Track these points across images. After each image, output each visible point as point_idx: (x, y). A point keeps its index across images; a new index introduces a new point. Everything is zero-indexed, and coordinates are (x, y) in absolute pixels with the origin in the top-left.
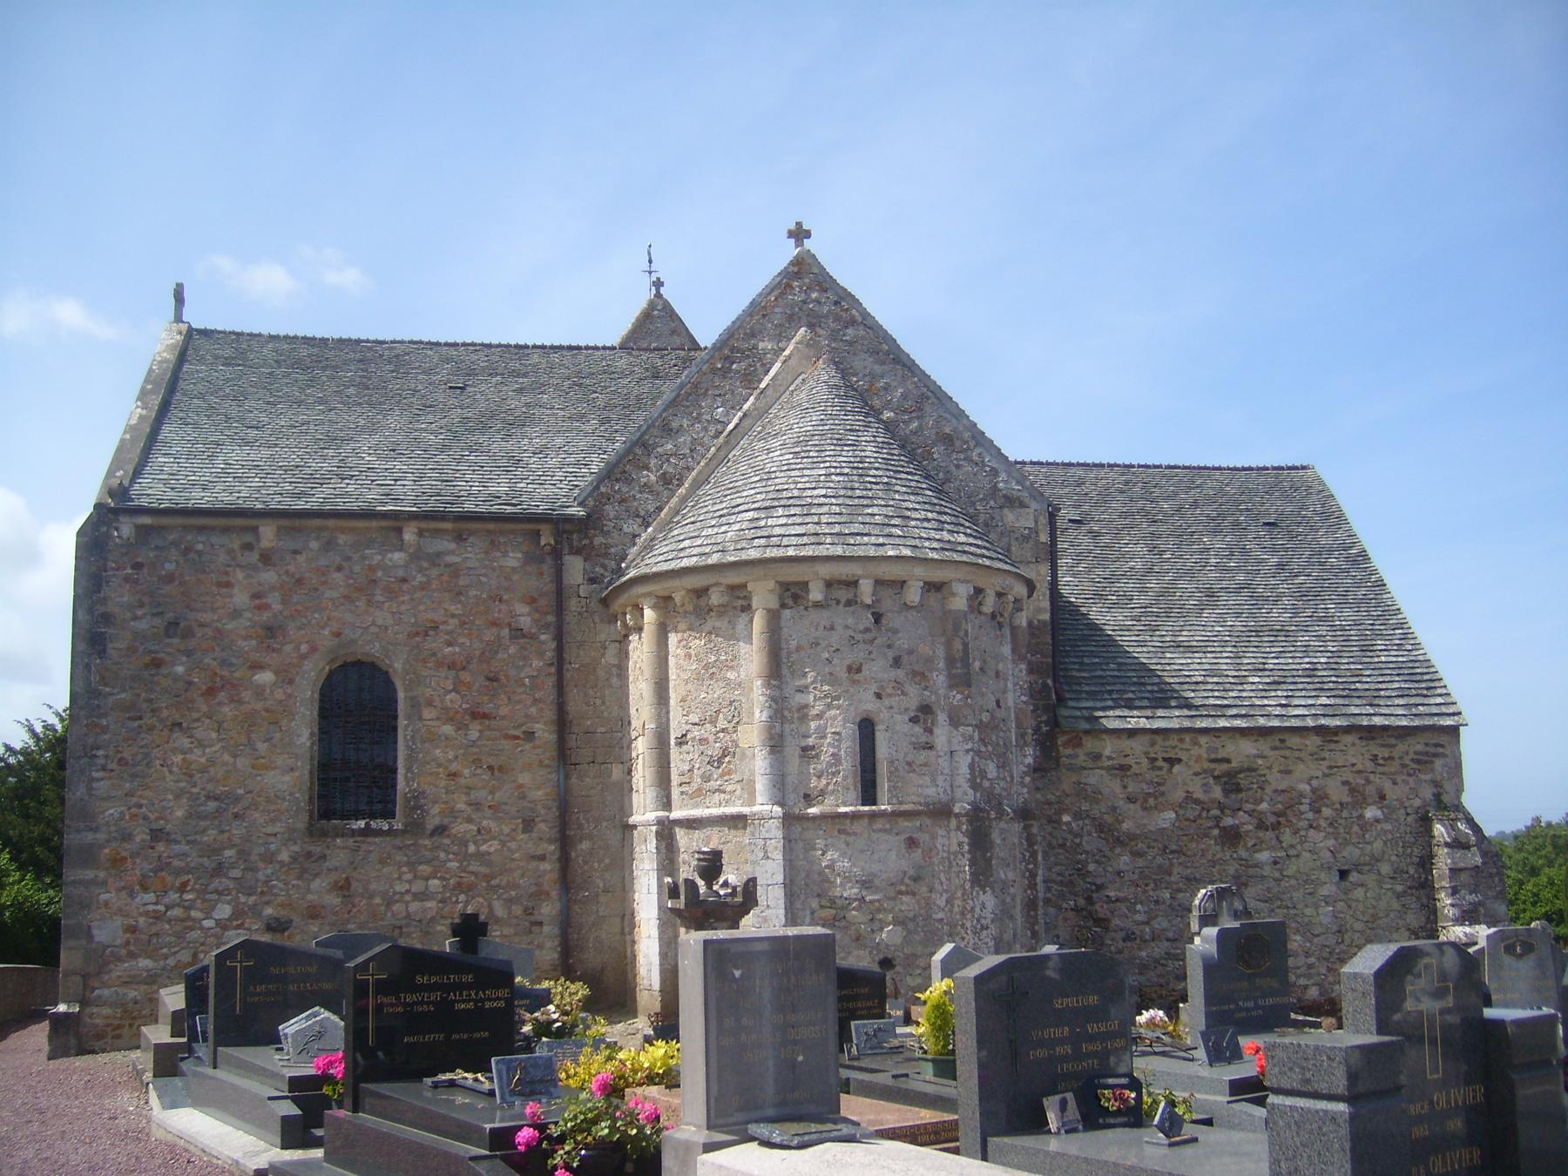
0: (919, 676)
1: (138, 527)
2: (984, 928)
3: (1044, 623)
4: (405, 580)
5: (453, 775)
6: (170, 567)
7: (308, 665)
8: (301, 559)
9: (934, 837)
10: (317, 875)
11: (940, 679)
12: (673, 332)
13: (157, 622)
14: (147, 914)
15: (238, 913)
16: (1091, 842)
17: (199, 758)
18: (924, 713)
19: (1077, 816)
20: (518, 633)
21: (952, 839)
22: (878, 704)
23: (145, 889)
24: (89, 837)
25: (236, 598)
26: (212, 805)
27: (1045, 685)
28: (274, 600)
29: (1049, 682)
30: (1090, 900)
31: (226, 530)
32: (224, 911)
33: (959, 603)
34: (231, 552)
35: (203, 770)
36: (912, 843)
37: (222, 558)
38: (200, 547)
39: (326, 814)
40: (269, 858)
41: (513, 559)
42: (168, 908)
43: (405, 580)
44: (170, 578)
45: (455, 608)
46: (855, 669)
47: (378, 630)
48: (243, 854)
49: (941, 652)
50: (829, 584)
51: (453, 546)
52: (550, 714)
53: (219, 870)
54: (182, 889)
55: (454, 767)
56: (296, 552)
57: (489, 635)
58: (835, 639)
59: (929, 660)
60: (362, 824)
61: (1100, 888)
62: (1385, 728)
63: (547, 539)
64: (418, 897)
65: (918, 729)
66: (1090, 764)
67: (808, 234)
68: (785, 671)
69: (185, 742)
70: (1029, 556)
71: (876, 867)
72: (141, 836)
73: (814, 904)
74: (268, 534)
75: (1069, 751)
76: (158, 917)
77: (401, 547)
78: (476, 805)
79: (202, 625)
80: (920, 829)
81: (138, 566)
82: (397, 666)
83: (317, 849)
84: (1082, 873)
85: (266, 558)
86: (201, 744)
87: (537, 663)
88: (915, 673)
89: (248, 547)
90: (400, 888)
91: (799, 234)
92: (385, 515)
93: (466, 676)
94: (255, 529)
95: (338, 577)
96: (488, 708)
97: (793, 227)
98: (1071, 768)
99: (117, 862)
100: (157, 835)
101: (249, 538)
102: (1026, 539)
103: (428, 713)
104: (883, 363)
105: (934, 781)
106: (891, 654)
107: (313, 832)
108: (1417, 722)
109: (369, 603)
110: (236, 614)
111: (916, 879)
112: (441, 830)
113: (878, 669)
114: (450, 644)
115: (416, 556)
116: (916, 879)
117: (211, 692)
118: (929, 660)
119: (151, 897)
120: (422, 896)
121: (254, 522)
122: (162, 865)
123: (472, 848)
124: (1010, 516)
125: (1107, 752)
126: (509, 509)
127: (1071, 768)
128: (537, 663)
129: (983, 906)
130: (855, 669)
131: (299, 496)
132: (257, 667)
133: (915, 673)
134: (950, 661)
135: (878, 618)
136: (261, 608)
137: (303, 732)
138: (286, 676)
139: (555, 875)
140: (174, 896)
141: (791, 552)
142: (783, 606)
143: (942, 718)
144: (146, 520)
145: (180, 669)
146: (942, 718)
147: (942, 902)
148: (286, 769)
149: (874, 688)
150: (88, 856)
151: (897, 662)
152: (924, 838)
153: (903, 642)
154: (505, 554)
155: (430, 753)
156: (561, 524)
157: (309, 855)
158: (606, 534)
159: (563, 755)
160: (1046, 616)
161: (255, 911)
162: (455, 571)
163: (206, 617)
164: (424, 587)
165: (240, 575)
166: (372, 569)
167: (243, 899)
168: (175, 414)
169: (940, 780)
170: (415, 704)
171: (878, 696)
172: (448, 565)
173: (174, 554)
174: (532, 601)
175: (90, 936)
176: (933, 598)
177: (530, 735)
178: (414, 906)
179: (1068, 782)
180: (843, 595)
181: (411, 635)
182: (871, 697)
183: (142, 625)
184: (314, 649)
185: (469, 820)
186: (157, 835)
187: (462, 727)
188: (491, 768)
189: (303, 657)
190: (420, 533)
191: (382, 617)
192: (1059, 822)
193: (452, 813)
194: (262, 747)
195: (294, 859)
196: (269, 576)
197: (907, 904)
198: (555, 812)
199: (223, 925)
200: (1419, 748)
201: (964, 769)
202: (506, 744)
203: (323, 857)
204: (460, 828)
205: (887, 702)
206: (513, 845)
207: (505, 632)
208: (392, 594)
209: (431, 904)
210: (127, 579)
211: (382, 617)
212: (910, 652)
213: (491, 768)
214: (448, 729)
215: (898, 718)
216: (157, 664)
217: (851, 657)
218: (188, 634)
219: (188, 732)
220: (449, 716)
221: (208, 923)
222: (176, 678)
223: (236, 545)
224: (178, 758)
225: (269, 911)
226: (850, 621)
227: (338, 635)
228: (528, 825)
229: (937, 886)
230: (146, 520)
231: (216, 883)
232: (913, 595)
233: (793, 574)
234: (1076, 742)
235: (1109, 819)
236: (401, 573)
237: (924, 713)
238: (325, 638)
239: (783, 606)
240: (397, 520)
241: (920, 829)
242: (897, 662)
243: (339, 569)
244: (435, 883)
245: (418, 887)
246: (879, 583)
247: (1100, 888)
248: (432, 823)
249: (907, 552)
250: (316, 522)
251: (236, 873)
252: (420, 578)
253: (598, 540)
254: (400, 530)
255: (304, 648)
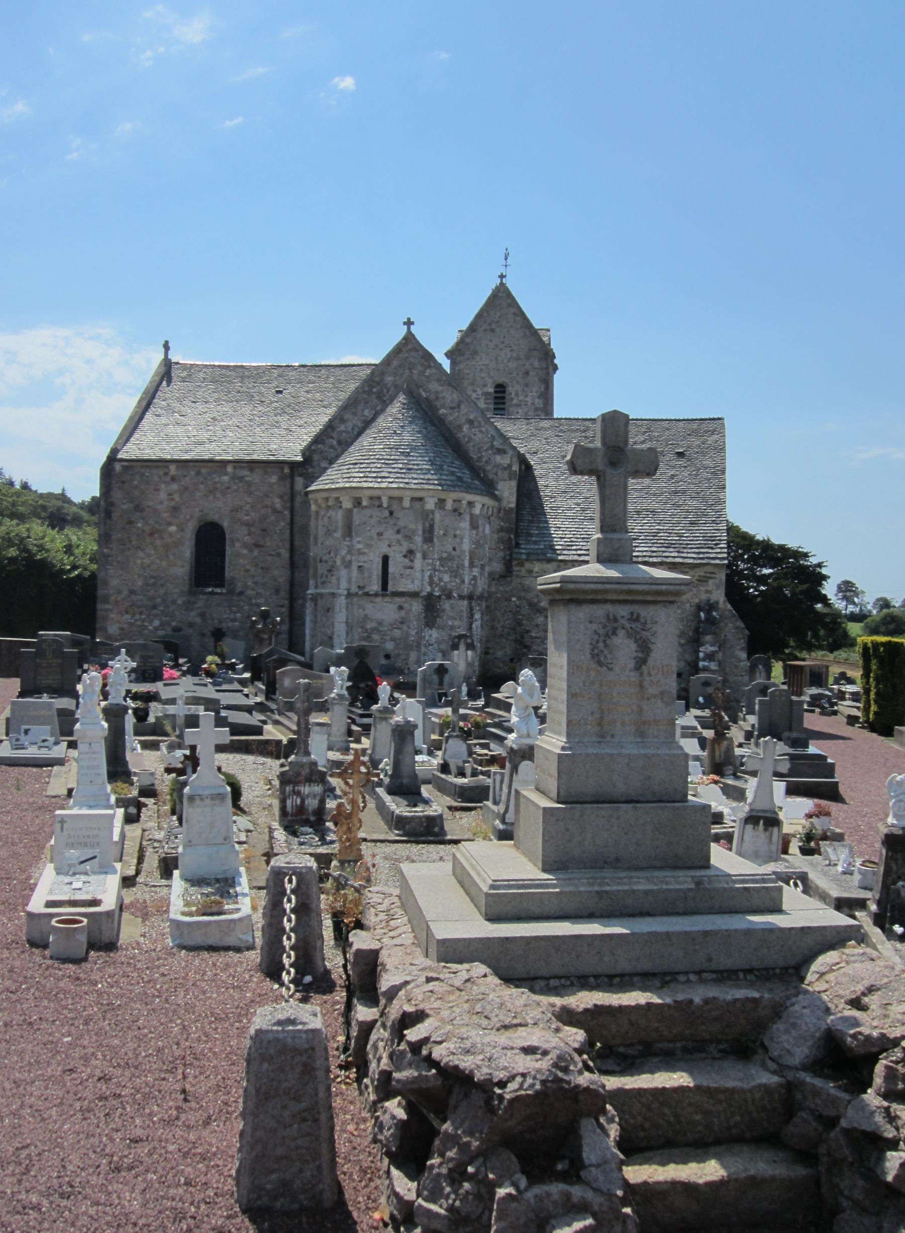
0: (409, 538)
1: (123, 466)
2: (430, 645)
3: (511, 509)
4: (228, 488)
5: (247, 571)
6: (135, 482)
7: (190, 524)
8: (187, 479)
9: (411, 605)
10: (193, 609)
11: (419, 539)
12: (509, 306)
13: (131, 505)
14: (128, 623)
15: (162, 624)
16: (526, 610)
17: (147, 561)
18: (410, 553)
19: (519, 598)
20: (275, 511)
21: (417, 607)
22: (389, 549)
23: (127, 613)
24: (106, 592)
25: (161, 497)
26: (152, 581)
27: (510, 538)
28: (176, 497)
29: (512, 536)
30: (522, 637)
31: (158, 467)
32: (157, 623)
33: (430, 504)
34: (160, 477)
35: (149, 566)
36: (401, 608)
37: (156, 479)
38: (147, 474)
39: (198, 585)
40: (174, 602)
41: (274, 479)
42: (136, 621)
43: (228, 488)
44: (136, 487)
45: (249, 500)
46: (380, 534)
47: (217, 509)
48: (164, 600)
49: (420, 527)
50: (371, 498)
51: (248, 473)
52: (288, 546)
53: (154, 607)
54: (141, 613)
55: (248, 567)
56: (185, 476)
57: (263, 512)
58: (373, 521)
59: (414, 532)
60: (210, 590)
61: (528, 632)
62: (682, 564)
63: (287, 470)
64: (233, 620)
65: (406, 560)
66: (527, 575)
67: (413, 323)
68: (354, 534)
69: (141, 554)
70: (506, 477)
71: (384, 617)
72: (126, 592)
73: (360, 630)
74: (173, 469)
75: (517, 568)
76: (131, 624)
77: (226, 474)
78: (256, 583)
79: (149, 507)
80: (405, 602)
81: (123, 482)
82: (225, 524)
83: (193, 599)
84: (519, 623)
85: (173, 479)
86: (149, 556)
87: (283, 524)
88: (406, 536)
89: (166, 474)
90: (225, 616)
91: (502, 277)
92: (217, 461)
93: (253, 529)
94: (167, 467)
95: (201, 486)
96: (262, 543)
97: (406, 320)
98: (518, 576)
99: (116, 602)
100: (132, 592)
101: (166, 470)
102: (505, 469)
103: (237, 545)
104: (442, 386)
105: (413, 582)
106: (396, 529)
107: (191, 593)
108: (699, 561)
109: (214, 497)
110: (161, 502)
111: (402, 623)
112: (241, 593)
113: (390, 534)
114: (247, 515)
115: (233, 478)
116: (402, 623)
117: (151, 534)
118: (414, 532)
119: (128, 616)
120: (233, 620)
121: (167, 464)
122: (134, 604)
123: (254, 601)
124: (498, 458)
125: (536, 569)
126: (272, 458)
127: (518, 576)
128: (283, 524)
129: (431, 636)
130: (380, 534)
131: (187, 452)
132: (170, 524)
133: (406, 536)
134: (424, 531)
135: (391, 513)
136: (171, 500)
137: (188, 551)
138: (181, 529)
139: (287, 613)
140: (137, 616)
141: (354, 485)
142: (355, 507)
143: (419, 555)
144: (125, 464)
145: (140, 525)
146: (419, 555)
147: (414, 633)
148: (180, 565)
149: (387, 543)
150: (106, 600)
151: (398, 532)
152: (406, 606)
153: (401, 523)
154: (270, 476)
155: (239, 559)
156: (293, 465)
157: (189, 602)
158: (312, 467)
159: (292, 564)
160: (513, 505)
161: (168, 624)
162: (249, 484)
163: (150, 504)
164: (236, 491)
165: (163, 486)
166: (216, 483)
167: (164, 618)
168: (152, 409)
169: (416, 582)
170: (232, 540)
171: (389, 546)
172: (247, 482)
173: (137, 477)
174: (281, 497)
175: (107, 631)
176: (417, 505)
177: (279, 555)
178: (230, 624)
179: (516, 582)
180: (377, 503)
181: (232, 511)
182: (386, 546)
183: (125, 507)
184: (192, 517)
185: (253, 590)
186: (132, 592)
187: (251, 551)
188: (262, 568)
189: (188, 520)
190: (235, 468)
191: (220, 504)
192: (510, 600)
193: (246, 586)
194: (172, 557)
195: (184, 602)
196: (175, 487)
197: (397, 633)
198: (288, 587)
199: (156, 629)
200: (702, 574)
201: (427, 578)
202: (269, 558)
203: (195, 603)
204: (249, 592)
205: (393, 548)
206: (270, 600)
207: (270, 510)
208: (224, 494)
209: (237, 623)
210: (119, 488)
211: (220, 504)
212: (405, 527)
213: (262, 568)
214: (245, 551)
215: (397, 555)
216: (131, 522)
217: (379, 529)
218: (143, 510)
219: (143, 550)
220: (245, 546)
221: (150, 628)
222: (138, 528)
223: (161, 473)
224: (139, 561)
225: (174, 624)
226: (379, 514)
227: (202, 511)
228: (277, 591)
229: (412, 626)
230: (125, 464)
231: (154, 612)
232: (406, 503)
233: (358, 494)
234: (521, 564)
235: (535, 600)
236: (227, 485)
237: (410, 553)
238: (197, 513)
239: (355, 507)
240: (224, 463)
241: (405, 602)
242: (398, 532)
243: (202, 483)
244: (238, 615)
245: (232, 616)
246: (390, 498)
247: (528, 632)
248: (239, 589)
249: (402, 485)
250: (192, 464)
251: (161, 608)
252: (235, 487)
253: (310, 470)
254: (226, 467)
255: (188, 517)
